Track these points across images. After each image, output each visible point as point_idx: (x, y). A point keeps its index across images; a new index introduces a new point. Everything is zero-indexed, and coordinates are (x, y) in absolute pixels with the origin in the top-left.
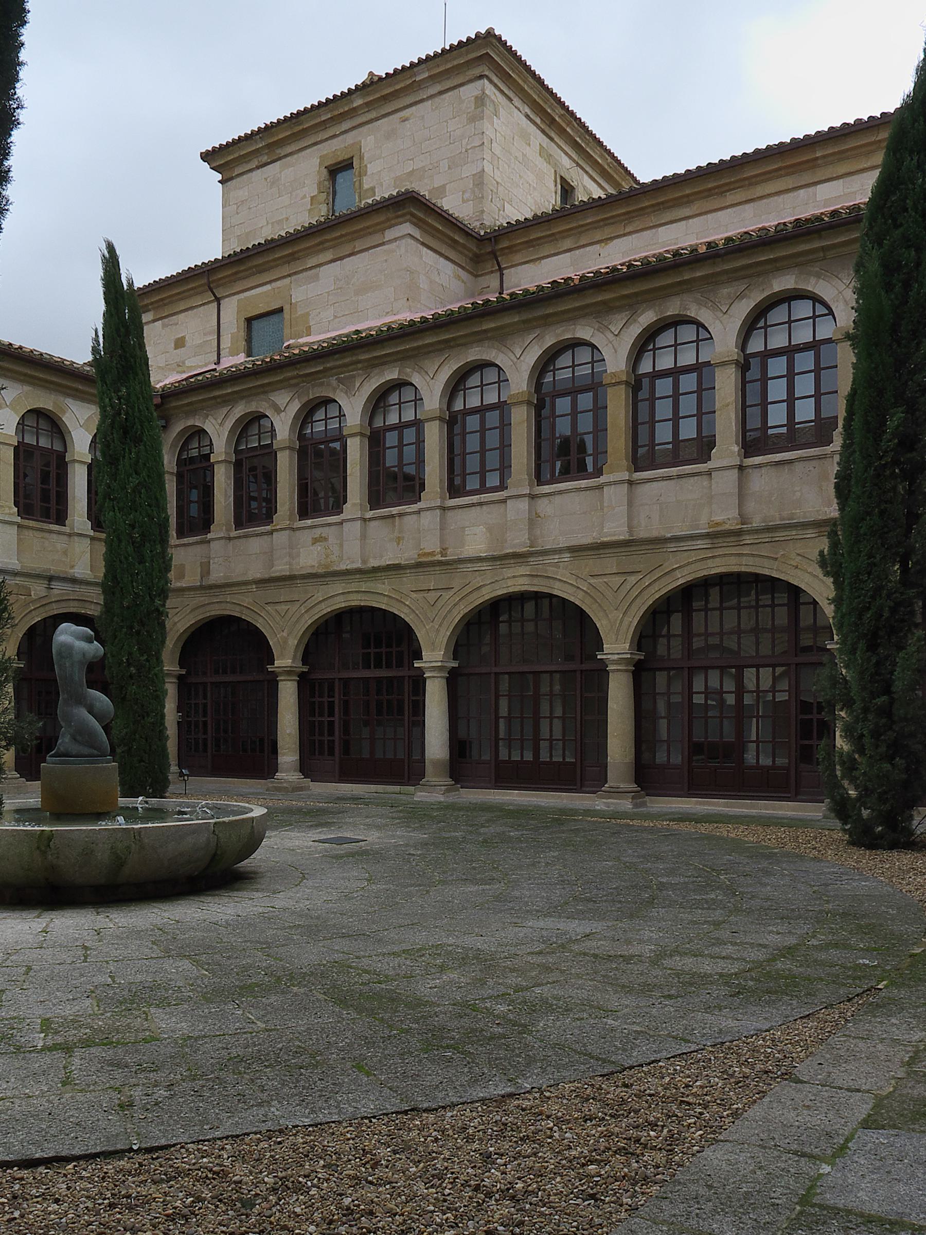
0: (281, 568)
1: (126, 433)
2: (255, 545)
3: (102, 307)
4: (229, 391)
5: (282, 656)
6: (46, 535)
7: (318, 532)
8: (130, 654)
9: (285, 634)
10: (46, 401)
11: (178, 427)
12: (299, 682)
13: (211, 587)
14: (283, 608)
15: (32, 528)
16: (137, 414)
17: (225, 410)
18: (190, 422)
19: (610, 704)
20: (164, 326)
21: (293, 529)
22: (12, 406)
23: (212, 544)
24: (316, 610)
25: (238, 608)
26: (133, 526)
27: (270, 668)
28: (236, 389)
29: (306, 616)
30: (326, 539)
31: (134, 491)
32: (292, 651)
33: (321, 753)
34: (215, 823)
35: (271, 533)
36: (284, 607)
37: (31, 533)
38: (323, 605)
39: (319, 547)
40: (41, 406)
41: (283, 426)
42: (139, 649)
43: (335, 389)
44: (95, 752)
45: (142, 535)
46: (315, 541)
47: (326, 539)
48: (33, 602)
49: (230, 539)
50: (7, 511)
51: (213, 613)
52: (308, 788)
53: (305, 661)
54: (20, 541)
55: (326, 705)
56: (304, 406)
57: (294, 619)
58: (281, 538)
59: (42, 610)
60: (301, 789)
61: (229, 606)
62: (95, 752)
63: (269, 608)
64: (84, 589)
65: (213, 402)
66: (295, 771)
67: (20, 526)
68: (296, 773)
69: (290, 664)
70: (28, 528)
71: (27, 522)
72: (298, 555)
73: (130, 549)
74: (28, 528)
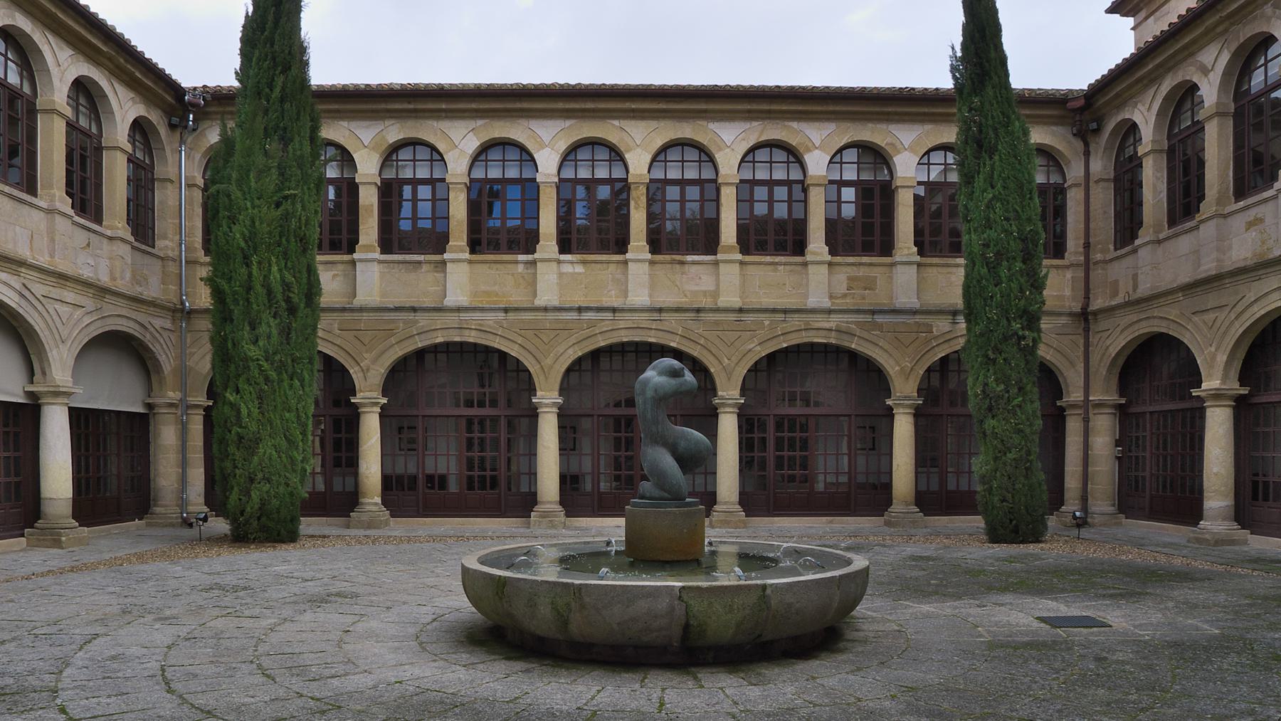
0: (1208, 267)
1: (980, 146)
2: (1184, 244)
3: (961, 18)
4: (1150, 66)
5: (1210, 376)
6: (950, 270)
7: (1252, 213)
8: (986, 384)
9: (1213, 349)
10: (774, 132)
11: (1110, 126)
12: (1234, 408)
13: (1139, 302)
14: (1210, 316)
15: (937, 265)
16: (990, 122)
17: (1152, 92)
18: (1120, 118)
19: (1068, 440)
20: (1156, 21)
21: (1225, 216)
22: (911, 149)
23: (1141, 252)
24: (1247, 315)
25: (1164, 323)
26: (986, 245)
27: (1195, 392)
28: (1157, 61)
29: (1237, 324)
30: (1261, 220)
31: (987, 207)
32: (1222, 367)
33: (1266, 499)
34: (683, 587)
35: (1197, 228)
36: (1212, 316)
37: (935, 270)
38: (1255, 308)
39: (1253, 234)
40: (945, 141)
41: (1210, 92)
42: (996, 380)
43: (1269, 19)
44: (666, 495)
45: (998, 254)
46: (1250, 225)
47: (1261, 220)
48: (936, 338)
49: (1159, 242)
50: (906, 252)
51: (1141, 332)
52: (1245, 542)
53: (1243, 380)
54: (743, 275)
55: (476, 442)
56: (1235, 56)
57: (1223, 329)
58: (1208, 231)
59: (946, 346)
60: (1232, 542)
61: (1156, 322)
62: (666, 495)
63: (1195, 318)
64: (636, 316)
65: (1140, 85)
66: (1224, 519)
67: (742, 263)
68: (1226, 523)
69: (1217, 386)
70: (839, 264)
71: (748, 258)
72: (1230, 248)
73: (984, 271)
74: (839, 264)
